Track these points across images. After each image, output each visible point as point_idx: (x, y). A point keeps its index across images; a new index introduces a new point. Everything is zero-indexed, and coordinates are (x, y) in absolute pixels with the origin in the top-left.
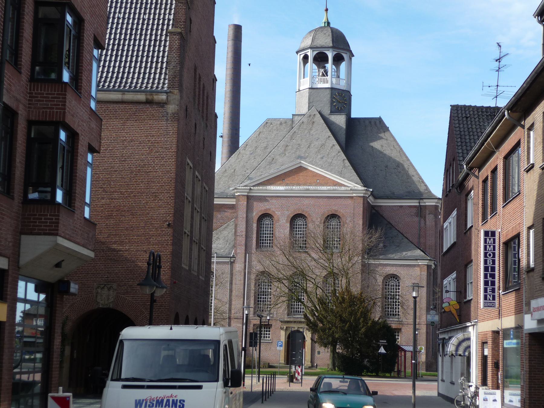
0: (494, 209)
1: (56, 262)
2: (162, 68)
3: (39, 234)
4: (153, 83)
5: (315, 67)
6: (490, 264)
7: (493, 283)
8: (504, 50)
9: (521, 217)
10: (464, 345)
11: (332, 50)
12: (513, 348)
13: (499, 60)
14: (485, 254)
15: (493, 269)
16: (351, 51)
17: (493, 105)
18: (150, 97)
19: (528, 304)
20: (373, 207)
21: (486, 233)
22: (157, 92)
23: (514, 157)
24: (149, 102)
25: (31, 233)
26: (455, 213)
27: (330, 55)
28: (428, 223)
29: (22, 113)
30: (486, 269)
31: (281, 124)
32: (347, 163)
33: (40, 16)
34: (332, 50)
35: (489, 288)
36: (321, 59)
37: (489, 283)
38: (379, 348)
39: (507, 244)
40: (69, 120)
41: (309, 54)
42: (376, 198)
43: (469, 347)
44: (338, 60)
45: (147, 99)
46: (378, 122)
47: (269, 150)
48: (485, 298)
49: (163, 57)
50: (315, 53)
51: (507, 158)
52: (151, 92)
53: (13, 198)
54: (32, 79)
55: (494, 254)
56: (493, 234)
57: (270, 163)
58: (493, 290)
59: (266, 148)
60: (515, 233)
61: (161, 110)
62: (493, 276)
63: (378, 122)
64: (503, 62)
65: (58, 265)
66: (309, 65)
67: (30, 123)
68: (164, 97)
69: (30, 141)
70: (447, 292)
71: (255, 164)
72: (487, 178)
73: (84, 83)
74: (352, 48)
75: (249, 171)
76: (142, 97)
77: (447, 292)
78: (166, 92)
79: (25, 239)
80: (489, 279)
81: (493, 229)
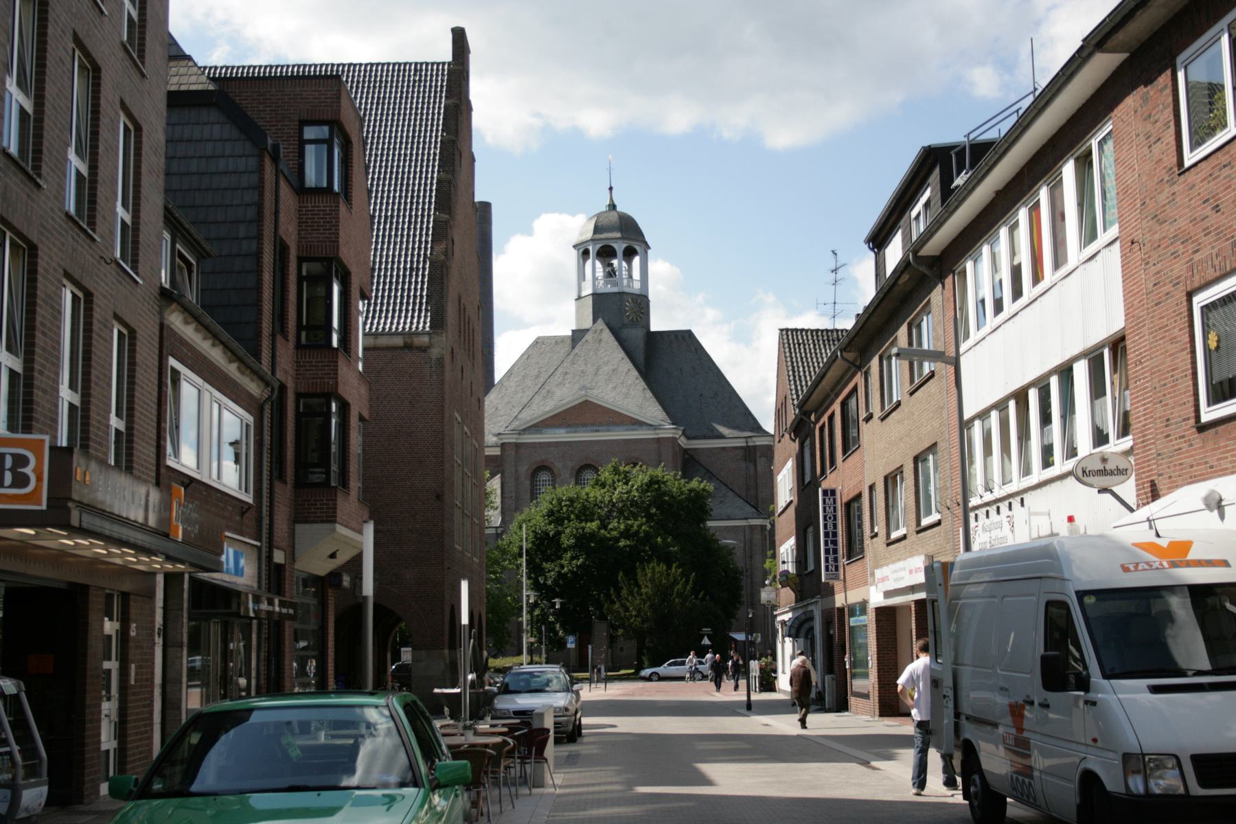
0: (833, 462)
1: (330, 552)
2: (421, 304)
3: (316, 522)
4: (412, 323)
5: (598, 264)
6: (830, 529)
7: (835, 551)
8: (841, 261)
9: (862, 473)
10: (807, 626)
11: (617, 239)
12: (376, 532)
13: (835, 271)
14: (825, 517)
15: (835, 534)
16: (646, 243)
17: (830, 327)
18: (409, 341)
19: (873, 574)
20: (686, 451)
21: (825, 492)
22: (417, 334)
23: (853, 402)
24: (408, 347)
25: (306, 521)
26: (937, 171)
27: (620, 247)
28: (759, 468)
29: (290, 385)
30: (826, 535)
31: (557, 343)
32: (649, 394)
33: (304, 273)
34: (617, 239)
35: (831, 557)
36: (606, 253)
37: (832, 551)
38: (703, 637)
39: (848, 505)
40: (343, 390)
41: (591, 248)
42: (689, 438)
43: (812, 629)
44: (629, 254)
45: (405, 343)
46: (687, 336)
47: (542, 380)
48: (827, 569)
49: (422, 289)
50: (598, 246)
51: (844, 404)
52: (410, 334)
53: (285, 483)
54: (299, 346)
55: (835, 517)
56: (833, 492)
57: (545, 397)
58: (836, 560)
59: (537, 377)
60: (856, 492)
61: (423, 355)
62: (835, 543)
63: (687, 336)
64: (840, 272)
65: (333, 556)
66: (589, 263)
67: (299, 396)
68: (426, 339)
69: (298, 415)
70: (784, 562)
71: (525, 400)
72: (824, 425)
73: (353, 345)
74: (647, 239)
75: (516, 411)
76: (399, 341)
77: (784, 562)
78: (428, 333)
79: (300, 528)
80: (831, 546)
81: (833, 486)
